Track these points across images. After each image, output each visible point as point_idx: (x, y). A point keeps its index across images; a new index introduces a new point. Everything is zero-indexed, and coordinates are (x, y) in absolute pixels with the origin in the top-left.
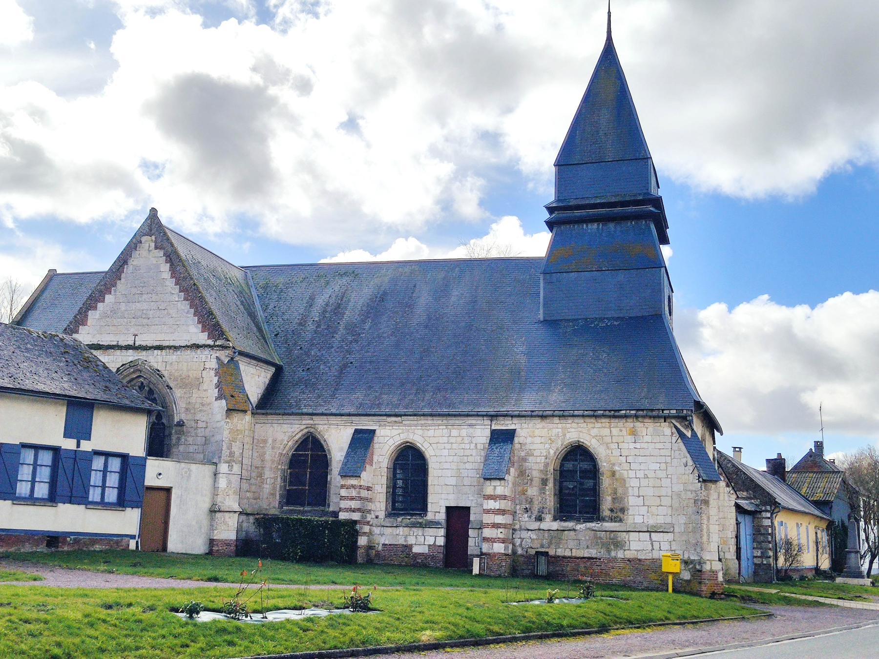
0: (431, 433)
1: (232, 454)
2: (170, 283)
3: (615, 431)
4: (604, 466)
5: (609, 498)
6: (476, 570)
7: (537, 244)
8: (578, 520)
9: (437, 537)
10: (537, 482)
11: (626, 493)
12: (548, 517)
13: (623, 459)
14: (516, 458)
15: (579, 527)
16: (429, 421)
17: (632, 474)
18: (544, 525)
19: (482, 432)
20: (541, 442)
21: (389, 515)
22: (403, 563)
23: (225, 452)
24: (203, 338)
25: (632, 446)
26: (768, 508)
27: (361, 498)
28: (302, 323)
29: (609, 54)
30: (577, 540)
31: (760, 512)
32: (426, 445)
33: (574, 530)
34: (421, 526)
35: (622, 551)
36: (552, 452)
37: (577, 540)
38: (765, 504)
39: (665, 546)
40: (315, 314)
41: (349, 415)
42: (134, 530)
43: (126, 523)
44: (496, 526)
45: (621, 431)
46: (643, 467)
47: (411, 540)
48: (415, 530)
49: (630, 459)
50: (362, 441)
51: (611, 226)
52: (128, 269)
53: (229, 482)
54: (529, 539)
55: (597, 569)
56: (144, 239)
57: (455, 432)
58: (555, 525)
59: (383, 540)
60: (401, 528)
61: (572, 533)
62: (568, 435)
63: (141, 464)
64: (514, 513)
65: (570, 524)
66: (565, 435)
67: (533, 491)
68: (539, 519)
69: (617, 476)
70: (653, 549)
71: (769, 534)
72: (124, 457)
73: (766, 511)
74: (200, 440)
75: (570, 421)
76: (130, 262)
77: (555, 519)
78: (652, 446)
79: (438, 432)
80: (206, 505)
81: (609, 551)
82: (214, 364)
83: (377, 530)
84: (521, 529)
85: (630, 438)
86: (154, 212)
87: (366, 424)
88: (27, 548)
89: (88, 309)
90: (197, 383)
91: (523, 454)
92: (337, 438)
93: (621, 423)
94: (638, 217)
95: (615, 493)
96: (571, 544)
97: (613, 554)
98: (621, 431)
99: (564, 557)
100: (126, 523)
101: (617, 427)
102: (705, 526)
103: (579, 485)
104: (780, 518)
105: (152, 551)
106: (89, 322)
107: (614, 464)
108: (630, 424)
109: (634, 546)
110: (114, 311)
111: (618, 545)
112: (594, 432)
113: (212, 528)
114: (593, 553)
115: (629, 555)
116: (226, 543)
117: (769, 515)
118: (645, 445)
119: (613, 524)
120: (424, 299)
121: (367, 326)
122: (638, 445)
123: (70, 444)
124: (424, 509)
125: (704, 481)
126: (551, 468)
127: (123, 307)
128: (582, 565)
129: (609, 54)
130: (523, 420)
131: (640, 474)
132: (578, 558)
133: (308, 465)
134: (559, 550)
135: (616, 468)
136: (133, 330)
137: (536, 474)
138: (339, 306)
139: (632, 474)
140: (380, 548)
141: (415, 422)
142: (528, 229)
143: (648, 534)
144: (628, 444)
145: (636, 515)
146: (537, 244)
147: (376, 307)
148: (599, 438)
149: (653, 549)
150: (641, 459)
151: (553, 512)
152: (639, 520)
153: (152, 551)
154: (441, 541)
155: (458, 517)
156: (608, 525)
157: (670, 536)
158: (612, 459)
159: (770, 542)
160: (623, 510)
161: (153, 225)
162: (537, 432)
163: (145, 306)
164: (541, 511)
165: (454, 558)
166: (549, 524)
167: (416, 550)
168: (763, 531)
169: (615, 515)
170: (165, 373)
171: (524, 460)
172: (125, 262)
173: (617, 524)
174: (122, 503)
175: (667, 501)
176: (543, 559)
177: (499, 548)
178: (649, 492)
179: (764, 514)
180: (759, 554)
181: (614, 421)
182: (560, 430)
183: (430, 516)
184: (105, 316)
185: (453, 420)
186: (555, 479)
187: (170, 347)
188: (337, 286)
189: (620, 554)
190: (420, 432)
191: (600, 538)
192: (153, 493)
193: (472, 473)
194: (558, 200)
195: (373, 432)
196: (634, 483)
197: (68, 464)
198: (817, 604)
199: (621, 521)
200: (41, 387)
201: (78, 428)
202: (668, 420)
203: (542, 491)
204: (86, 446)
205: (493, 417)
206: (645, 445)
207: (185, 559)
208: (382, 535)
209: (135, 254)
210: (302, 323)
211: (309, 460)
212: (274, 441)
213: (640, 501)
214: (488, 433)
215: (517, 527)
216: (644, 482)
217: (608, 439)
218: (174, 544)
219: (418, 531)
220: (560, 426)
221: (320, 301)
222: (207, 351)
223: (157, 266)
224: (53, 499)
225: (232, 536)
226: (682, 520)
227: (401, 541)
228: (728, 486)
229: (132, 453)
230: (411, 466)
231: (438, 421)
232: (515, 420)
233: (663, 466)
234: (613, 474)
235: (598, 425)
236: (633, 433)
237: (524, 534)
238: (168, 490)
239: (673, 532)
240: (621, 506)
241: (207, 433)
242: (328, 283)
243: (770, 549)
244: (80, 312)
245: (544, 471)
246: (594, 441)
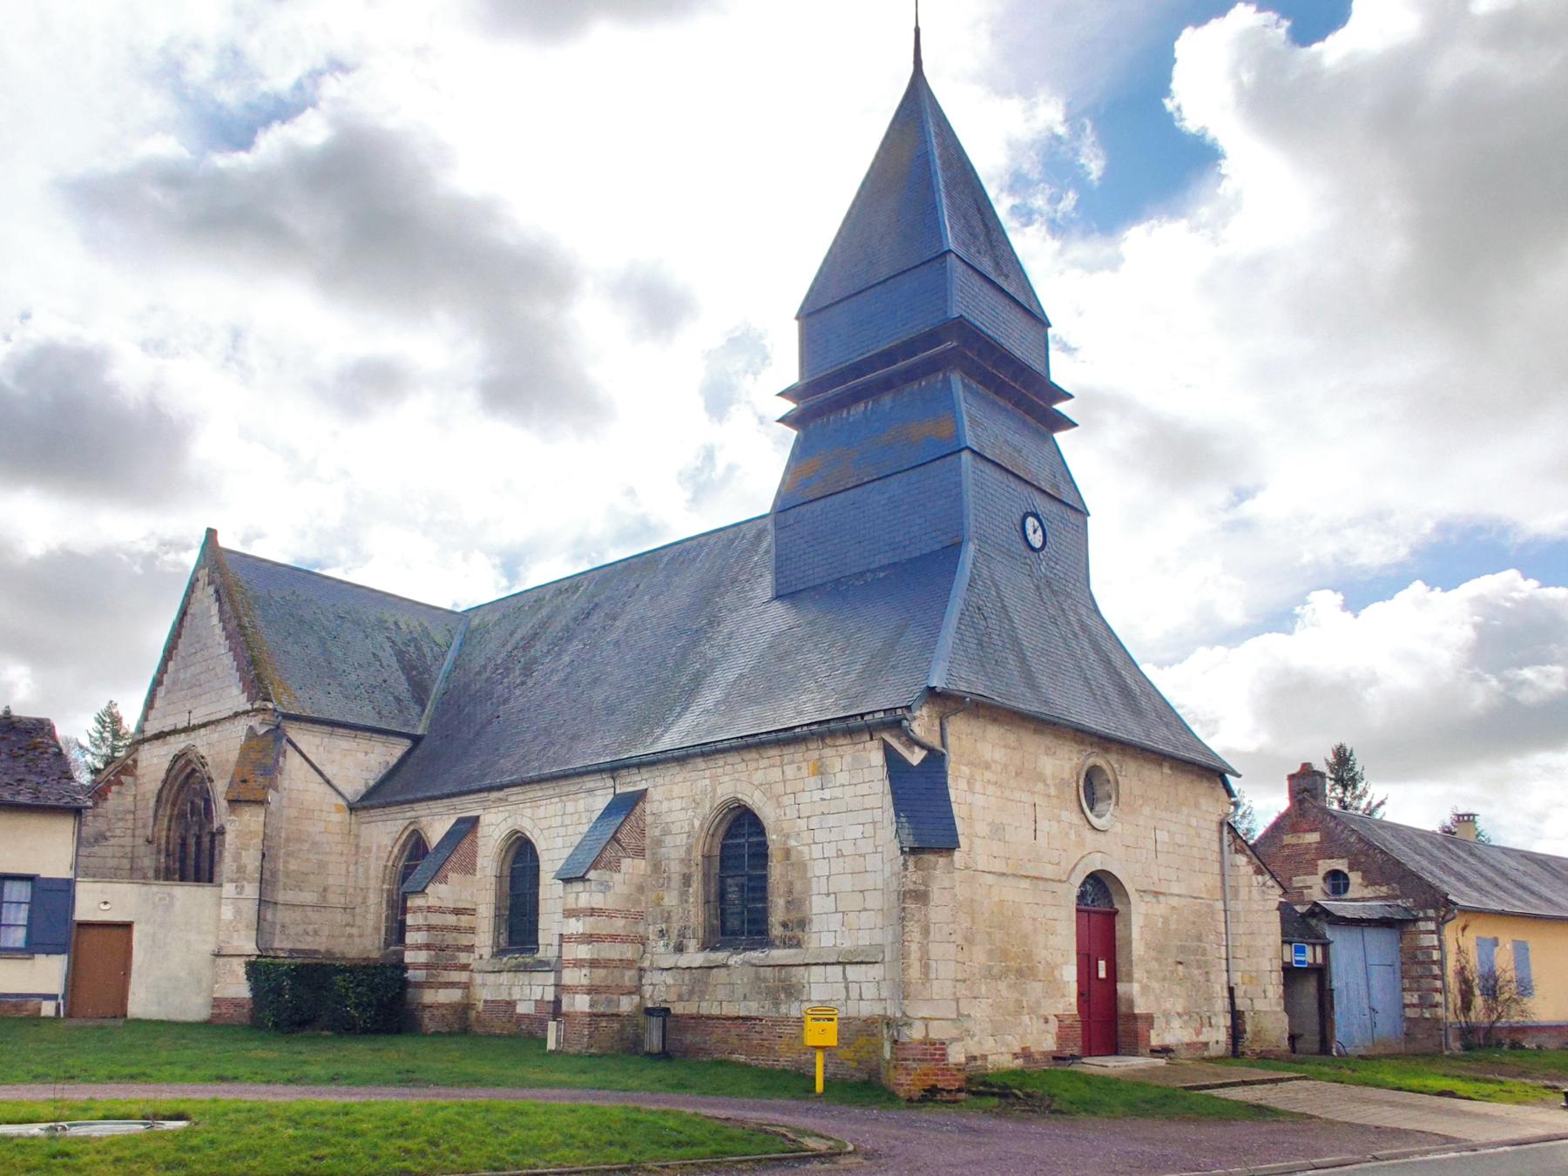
0: (541, 812)
1: (241, 869)
3: (790, 771)
5: (781, 902)
10: (676, 881)
11: (807, 891)
12: (692, 944)
13: (802, 823)
14: (648, 841)
15: (735, 960)
17: (816, 851)
18: (684, 960)
21: (499, 953)
25: (817, 795)
26: (1431, 913)
27: (430, 928)
30: (731, 986)
31: (1416, 920)
32: (536, 833)
33: (726, 966)
35: (797, 1004)
36: (697, 823)
38: (1424, 907)
39: (869, 992)
41: (449, 796)
42: (56, 985)
45: (799, 769)
46: (834, 836)
48: (520, 975)
49: (814, 823)
51: (887, 400)
53: (238, 911)
55: (755, 1039)
60: (505, 975)
61: (723, 970)
62: (719, 792)
63: (65, 889)
64: (643, 941)
65: (720, 956)
66: (714, 790)
68: (680, 949)
69: (794, 857)
70: (848, 998)
71: (1434, 962)
73: (1430, 919)
75: (721, 763)
77: (705, 946)
78: (849, 791)
79: (551, 810)
81: (776, 1004)
83: (478, 978)
84: (653, 968)
85: (813, 782)
91: (657, 832)
94: (933, 366)
95: (790, 892)
96: (721, 993)
97: (783, 1009)
98: (799, 769)
99: (709, 1018)
101: (792, 762)
102: (914, 947)
104: (1450, 932)
107: (788, 836)
109: (817, 993)
111: (791, 991)
112: (758, 777)
114: (752, 1008)
117: (1432, 926)
118: (838, 792)
119: (787, 951)
122: (827, 794)
125: (913, 851)
126: (697, 855)
128: (734, 1032)
130: (655, 771)
131: (830, 851)
132: (728, 1018)
134: (704, 1004)
135: (792, 843)
137: (1325, 769)
139: (816, 851)
140: (480, 1006)
141: (521, 797)
143: (839, 968)
144: (811, 796)
145: (825, 935)
149: (848, 998)
150: (832, 821)
151: (700, 933)
152: (827, 940)
157: (875, 972)
158: (785, 825)
159: (1435, 977)
160: (802, 924)
162: (677, 790)
167: (521, 1009)
168: (1421, 957)
169: (789, 934)
170: (209, 760)
171: (658, 843)
173: (792, 951)
174: (32, 948)
176: (656, 1022)
178: (845, 883)
179: (1422, 925)
180: (1415, 1000)
182: (707, 782)
183: (540, 955)
186: (706, 876)
190: (528, 812)
191: (765, 980)
192: (93, 932)
195: (478, 818)
196: (820, 869)
198: (1260, 1111)
199: (798, 945)
202: (877, 736)
203: (684, 895)
205: (614, 769)
206: (838, 792)
208: (484, 985)
212: (379, 847)
213: (829, 903)
215: (646, 964)
216: (837, 866)
217: (779, 788)
219: (523, 978)
220: (707, 773)
223: (209, 608)
228: (1258, 872)
229: (46, 873)
232: (645, 773)
233: (869, 829)
234: (787, 853)
235: (764, 763)
236: (820, 770)
237: (657, 977)
238: (128, 926)
239: (882, 962)
240: (800, 916)
243: (1436, 990)
245: (686, 861)
246: (757, 794)
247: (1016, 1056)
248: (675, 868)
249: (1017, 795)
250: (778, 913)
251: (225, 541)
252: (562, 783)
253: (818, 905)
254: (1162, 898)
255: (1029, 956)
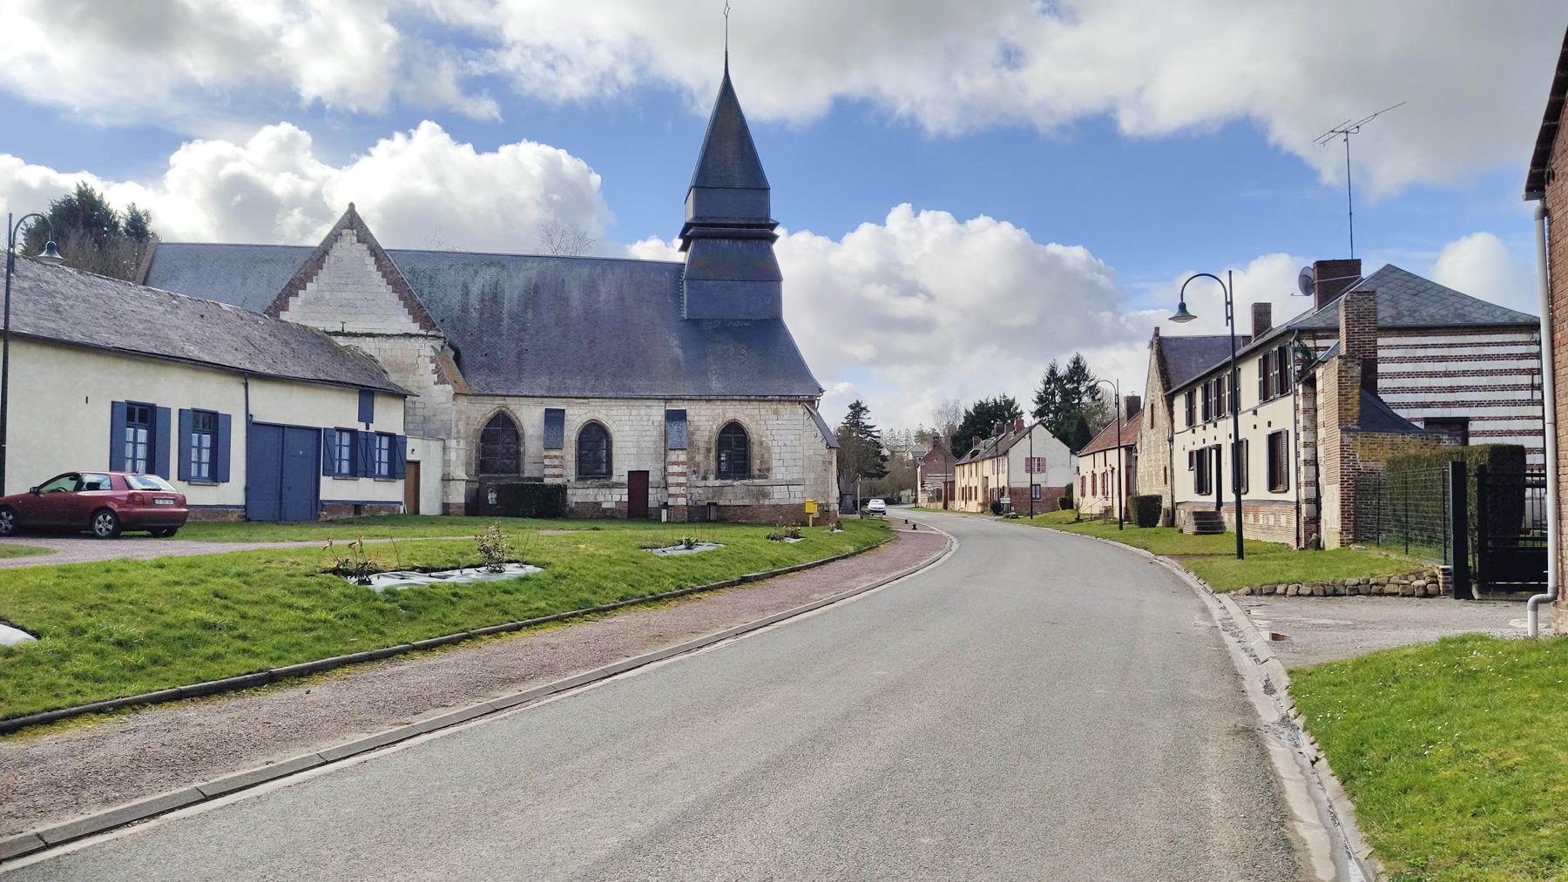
2: (377, 276)
4: (754, 437)
6: (664, 519)
7: (675, 254)
8: (734, 479)
9: (622, 495)
10: (703, 450)
11: (770, 458)
12: (712, 477)
16: (613, 402)
19: (657, 412)
20: (706, 419)
21: (578, 479)
22: (595, 515)
23: (454, 430)
24: (415, 328)
28: (465, 310)
29: (727, 90)
30: (735, 493)
34: (609, 487)
37: (735, 493)
40: (474, 301)
43: (393, 492)
44: (679, 485)
47: (600, 499)
50: (554, 419)
51: (740, 243)
52: (330, 260)
54: (701, 495)
56: (345, 232)
57: (634, 412)
58: (718, 483)
59: (575, 499)
63: (404, 440)
65: (729, 482)
67: (699, 458)
72: (392, 436)
74: (418, 419)
76: (332, 252)
80: (439, 475)
82: (429, 352)
86: (352, 205)
87: (557, 405)
88: (344, 516)
89: (288, 296)
90: (413, 368)
92: (530, 417)
93: (767, 405)
96: (730, 496)
100: (393, 492)
103: (735, 450)
105: (411, 513)
106: (291, 307)
108: (774, 406)
110: (318, 299)
111: (766, 495)
113: (445, 494)
114: (747, 502)
115: (773, 502)
116: (458, 506)
120: (576, 295)
121: (530, 315)
123: (361, 427)
124: (610, 473)
127: (327, 295)
129: (727, 90)
133: (500, 436)
136: (340, 318)
137: (702, 445)
138: (495, 296)
142: (667, 240)
144: (773, 422)
145: (778, 473)
146: (675, 254)
147: (533, 295)
148: (752, 417)
152: (779, 477)
153: (411, 513)
154: (625, 498)
155: (638, 480)
156: (757, 481)
160: (768, 470)
161: (352, 220)
163: (351, 295)
164: (706, 473)
165: (638, 509)
166: (713, 482)
167: (604, 506)
172: (326, 253)
174: (392, 475)
175: (800, 463)
177: (682, 501)
181: (763, 404)
183: (615, 479)
184: (307, 303)
185: (632, 402)
187: (382, 335)
188: (487, 276)
189: (767, 502)
193: (650, 445)
194: (696, 218)
196: (776, 450)
197: (363, 443)
200: (343, 379)
201: (366, 415)
204: (373, 429)
205: (666, 400)
207: (430, 520)
209: (336, 246)
210: (465, 310)
211: (500, 436)
214: (663, 412)
218: (423, 510)
221: (475, 290)
222: (421, 340)
224: (354, 474)
225: (462, 500)
226: (812, 475)
227: (592, 499)
230: (595, 440)
231: (620, 403)
236: (776, 412)
241: (426, 413)
242: (476, 273)
244: (279, 297)
248: (702, 445)
250: (756, 466)
251: (358, 210)
252: (215, 698)
253: (775, 463)
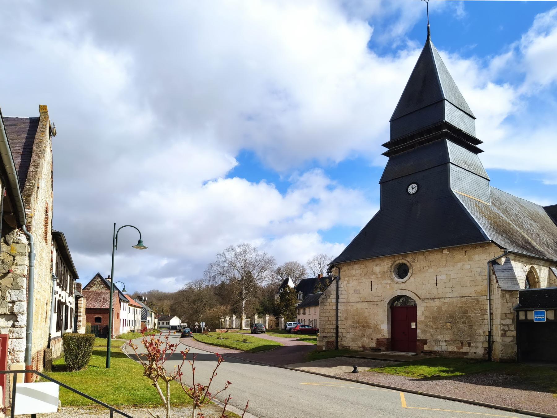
247: (360, 347)
249: (364, 280)
254: (436, 300)
255: (367, 322)
